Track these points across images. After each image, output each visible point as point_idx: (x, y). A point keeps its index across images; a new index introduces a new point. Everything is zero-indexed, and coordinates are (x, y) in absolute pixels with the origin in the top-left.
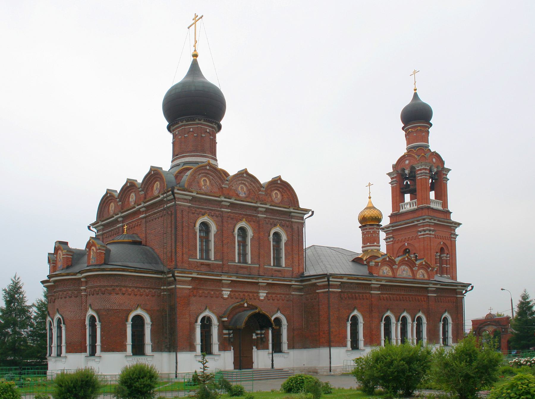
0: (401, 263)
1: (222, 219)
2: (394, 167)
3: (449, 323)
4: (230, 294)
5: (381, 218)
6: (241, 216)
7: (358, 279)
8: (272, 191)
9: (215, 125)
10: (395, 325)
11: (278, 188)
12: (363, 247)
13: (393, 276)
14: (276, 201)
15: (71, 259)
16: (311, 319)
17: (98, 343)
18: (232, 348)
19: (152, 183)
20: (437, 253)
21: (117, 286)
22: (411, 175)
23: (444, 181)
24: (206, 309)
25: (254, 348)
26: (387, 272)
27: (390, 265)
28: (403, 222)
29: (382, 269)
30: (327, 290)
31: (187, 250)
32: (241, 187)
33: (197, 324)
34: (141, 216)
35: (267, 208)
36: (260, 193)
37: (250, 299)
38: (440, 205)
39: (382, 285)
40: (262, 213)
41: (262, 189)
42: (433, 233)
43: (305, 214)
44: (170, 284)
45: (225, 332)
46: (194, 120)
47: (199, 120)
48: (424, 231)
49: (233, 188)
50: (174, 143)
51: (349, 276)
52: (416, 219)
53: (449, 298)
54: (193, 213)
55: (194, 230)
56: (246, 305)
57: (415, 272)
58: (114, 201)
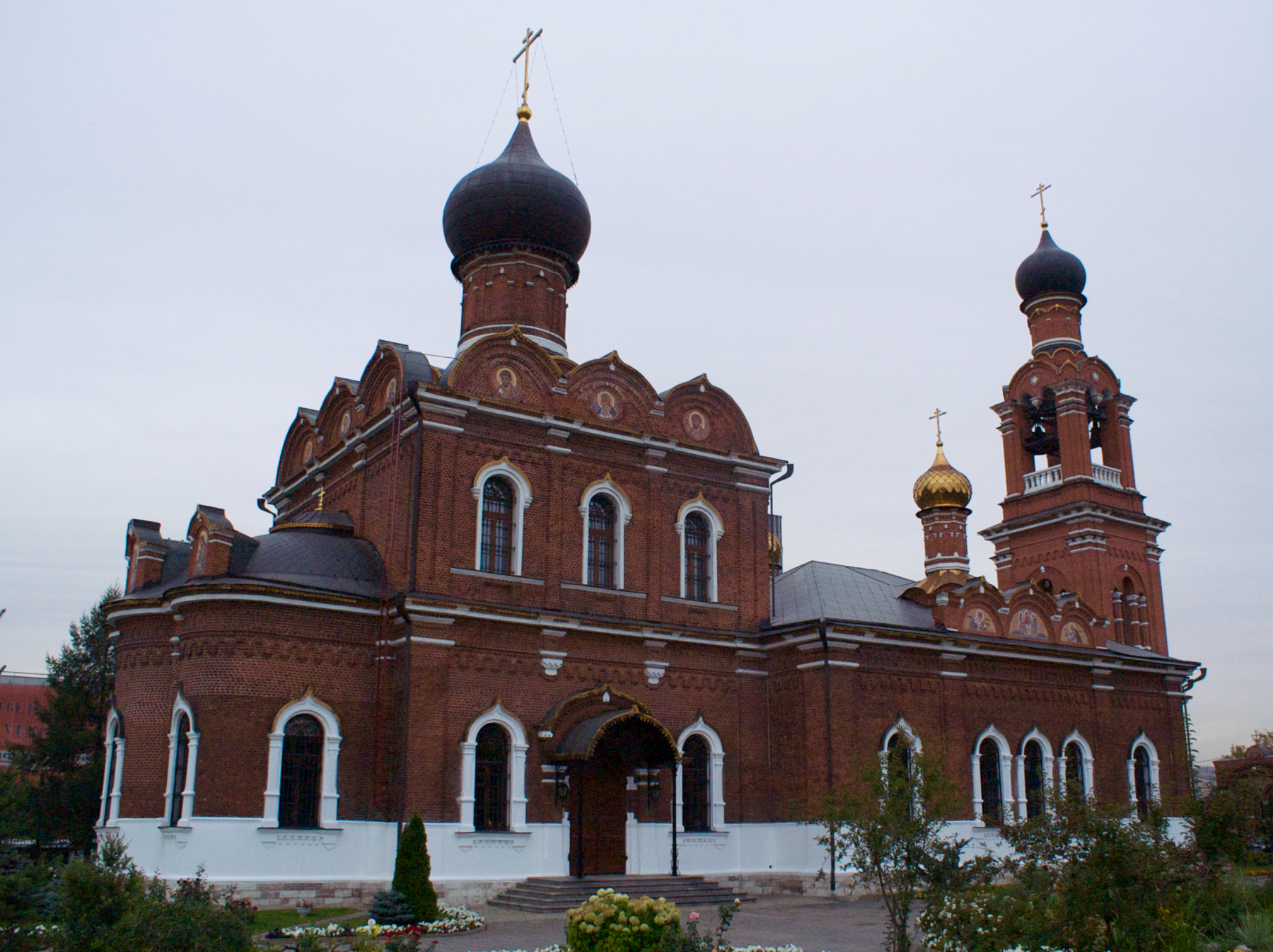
0: (1018, 603)
2: (1007, 391)
3: (1150, 763)
4: (563, 666)
5: (967, 493)
7: (903, 637)
8: (684, 411)
9: (561, 262)
10: (1009, 763)
11: (701, 406)
12: (927, 564)
13: (998, 635)
14: (696, 435)
16: (786, 742)
17: (189, 790)
18: (566, 815)
20: (1116, 590)
22: (1046, 409)
23: (1121, 423)
24: (493, 703)
25: (630, 815)
26: (982, 624)
27: (989, 606)
28: (1034, 518)
29: (969, 614)
30: (822, 663)
32: (603, 396)
33: (466, 743)
34: (355, 465)
36: (651, 412)
38: (1117, 478)
39: (969, 656)
40: (656, 461)
42: (1104, 542)
43: (772, 472)
44: (397, 633)
45: (546, 768)
46: (508, 249)
48: (1083, 536)
50: (464, 304)
51: (881, 629)
53: (1147, 699)
54: (469, 453)
55: (471, 494)
56: (606, 698)
57: (1056, 627)
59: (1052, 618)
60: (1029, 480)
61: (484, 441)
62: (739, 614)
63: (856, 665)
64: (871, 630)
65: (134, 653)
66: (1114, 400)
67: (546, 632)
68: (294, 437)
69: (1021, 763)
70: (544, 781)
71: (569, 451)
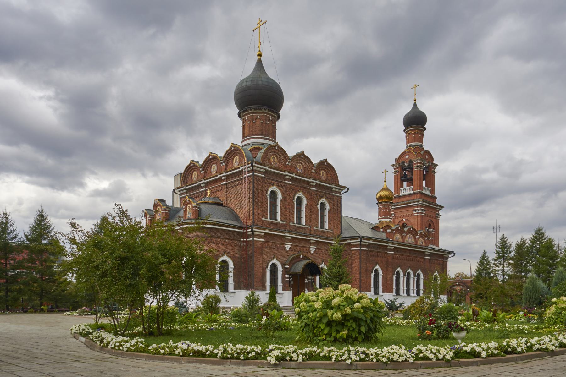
1: (286, 189)
2: (397, 160)
6: (298, 188)
8: (320, 170)
14: (323, 178)
15: (168, 214)
19: (232, 157)
20: (426, 227)
24: (274, 258)
30: (359, 248)
31: (261, 211)
34: (222, 183)
35: (317, 184)
37: (304, 252)
41: (314, 168)
43: (342, 190)
44: (248, 237)
45: (287, 276)
47: (265, 109)
49: (294, 166)
52: (413, 201)
54: (266, 183)
56: (301, 256)
57: (417, 240)
58: (196, 170)
59: (416, 237)
60: (402, 191)
61: (270, 179)
62: (333, 233)
63: (367, 249)
64: (372, 239)
66: (432, 165)
67: (286, 237)
68: (188, 170)
69: (405, 278)
71: (291, 183)
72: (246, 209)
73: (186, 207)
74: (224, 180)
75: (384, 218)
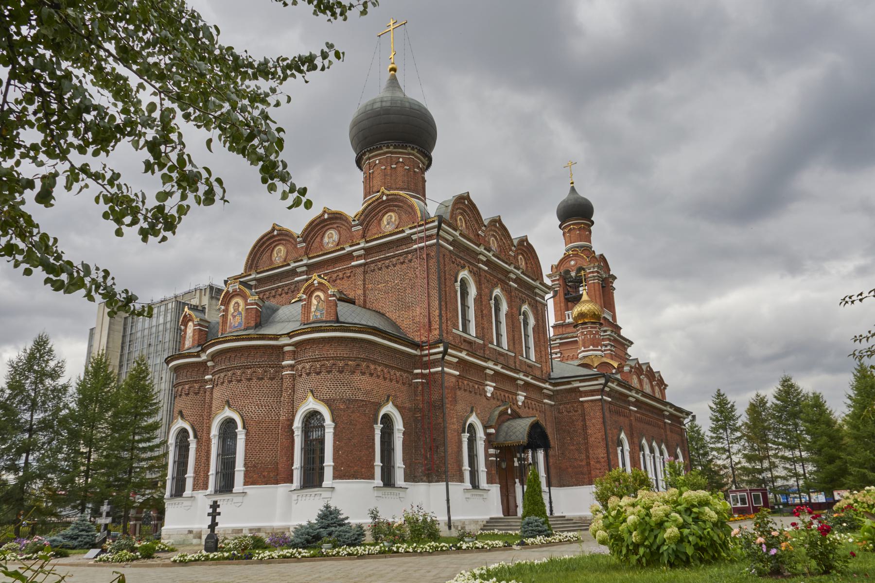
19: (380, 214)
21: (364, 360)
30: (600, 397)
34: (353, 263)
41: (513, 248)
44: (434, 363)
60: (569, 315)
65: (230, 373)
68: (264, 243)
70: (490, 459)
72: (419, 311)
73: (310, 296)
74: (359, 257)
75: (584, 351)
